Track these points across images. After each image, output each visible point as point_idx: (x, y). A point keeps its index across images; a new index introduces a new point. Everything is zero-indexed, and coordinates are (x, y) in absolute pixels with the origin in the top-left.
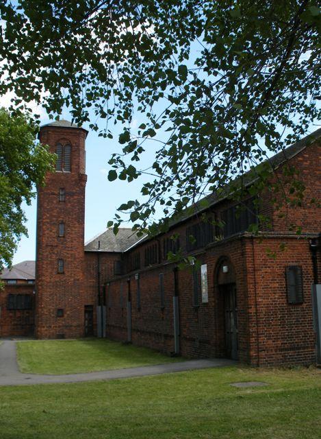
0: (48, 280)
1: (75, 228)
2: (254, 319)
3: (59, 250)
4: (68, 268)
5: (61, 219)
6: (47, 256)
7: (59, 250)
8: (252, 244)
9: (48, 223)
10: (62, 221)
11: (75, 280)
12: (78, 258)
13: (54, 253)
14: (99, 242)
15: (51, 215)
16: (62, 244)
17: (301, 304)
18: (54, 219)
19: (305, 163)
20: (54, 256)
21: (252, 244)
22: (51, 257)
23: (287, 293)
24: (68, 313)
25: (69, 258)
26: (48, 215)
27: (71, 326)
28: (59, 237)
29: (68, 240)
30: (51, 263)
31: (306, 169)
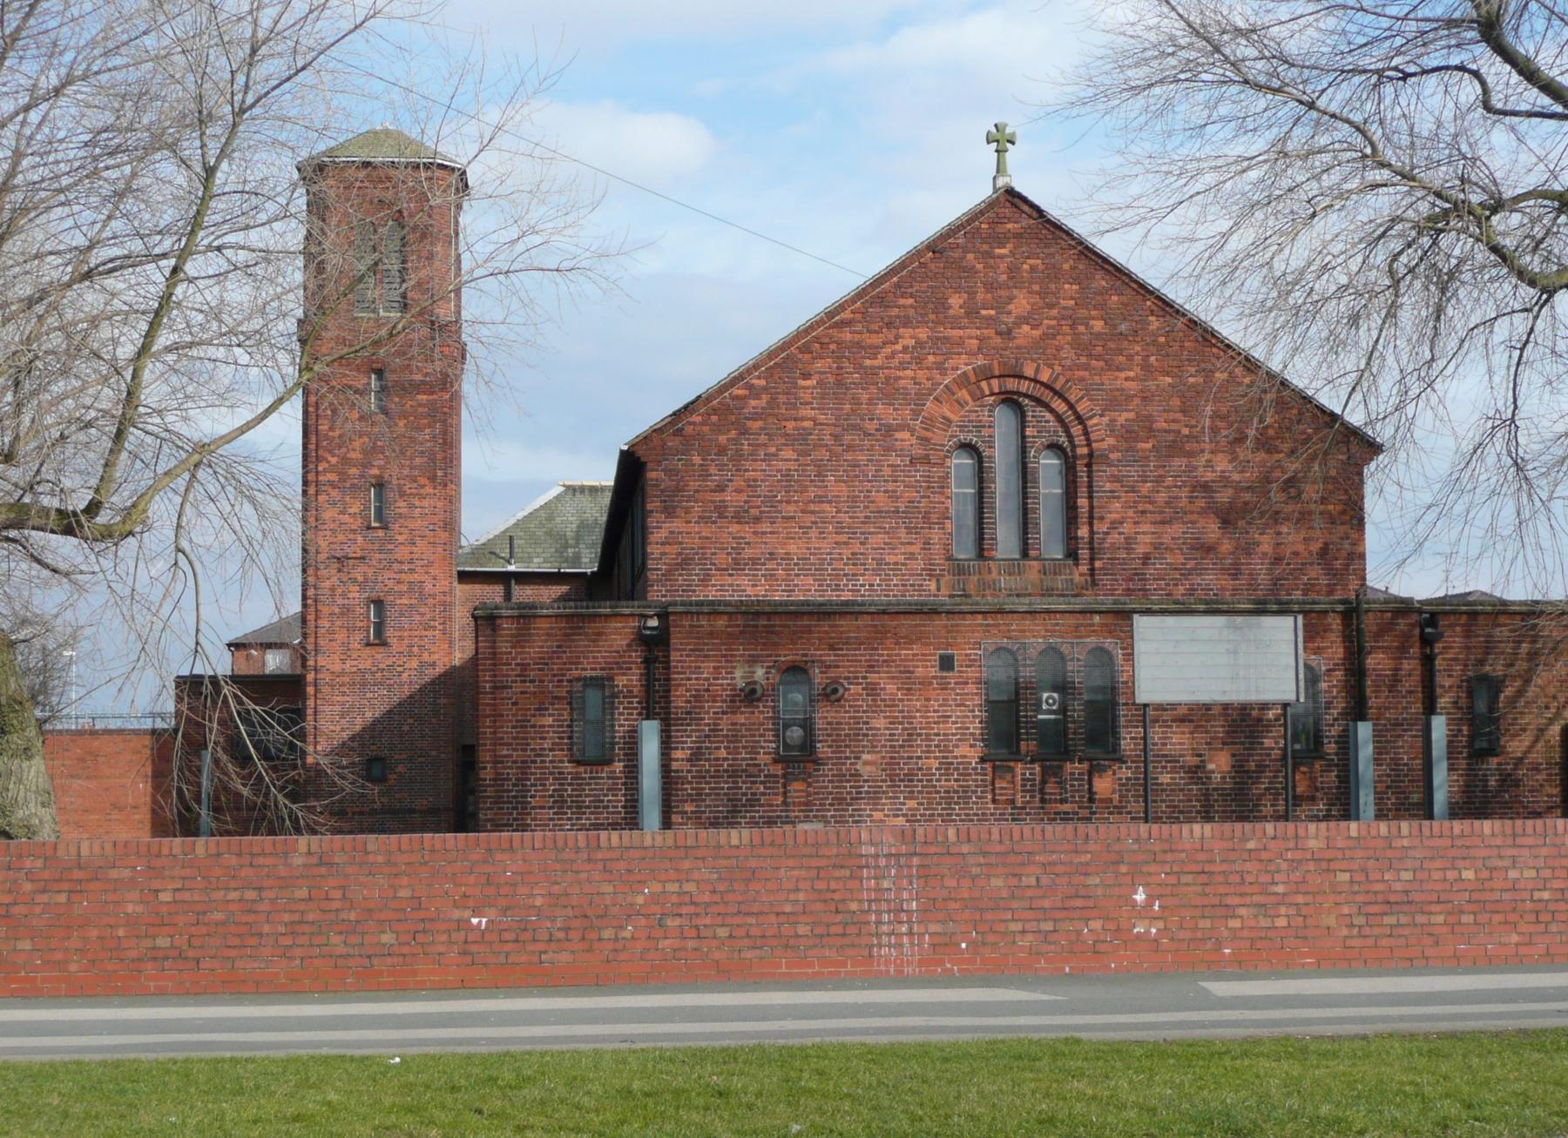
0: (337, 667)
1: (422, 497)
2: (490, 792)
3: (370, 572)
4: (402, 629)
5: (376, 471)
6: (333, 589)
7: (370, 572)
8: (494, 630)
9: (333, 485)
10: (381, 477)
11: (422, 664)
12: (433, 596)
13: (355, 581)
14: (511, 538)
15: (345, 460)
16: (380, 551)
17: (609, 762)
18: (353, 471)
19: (753, 403)
20: (355, 593)
21: (494, 630)
22: (343, 595)
23: (570, 738)
24: (400, 769)
25: (401, 594)
26: (334, 460)
27: (412, 811)
28: (369, 528)
29: (401, 539)
30: (346, 611)
31: (755, 417)
